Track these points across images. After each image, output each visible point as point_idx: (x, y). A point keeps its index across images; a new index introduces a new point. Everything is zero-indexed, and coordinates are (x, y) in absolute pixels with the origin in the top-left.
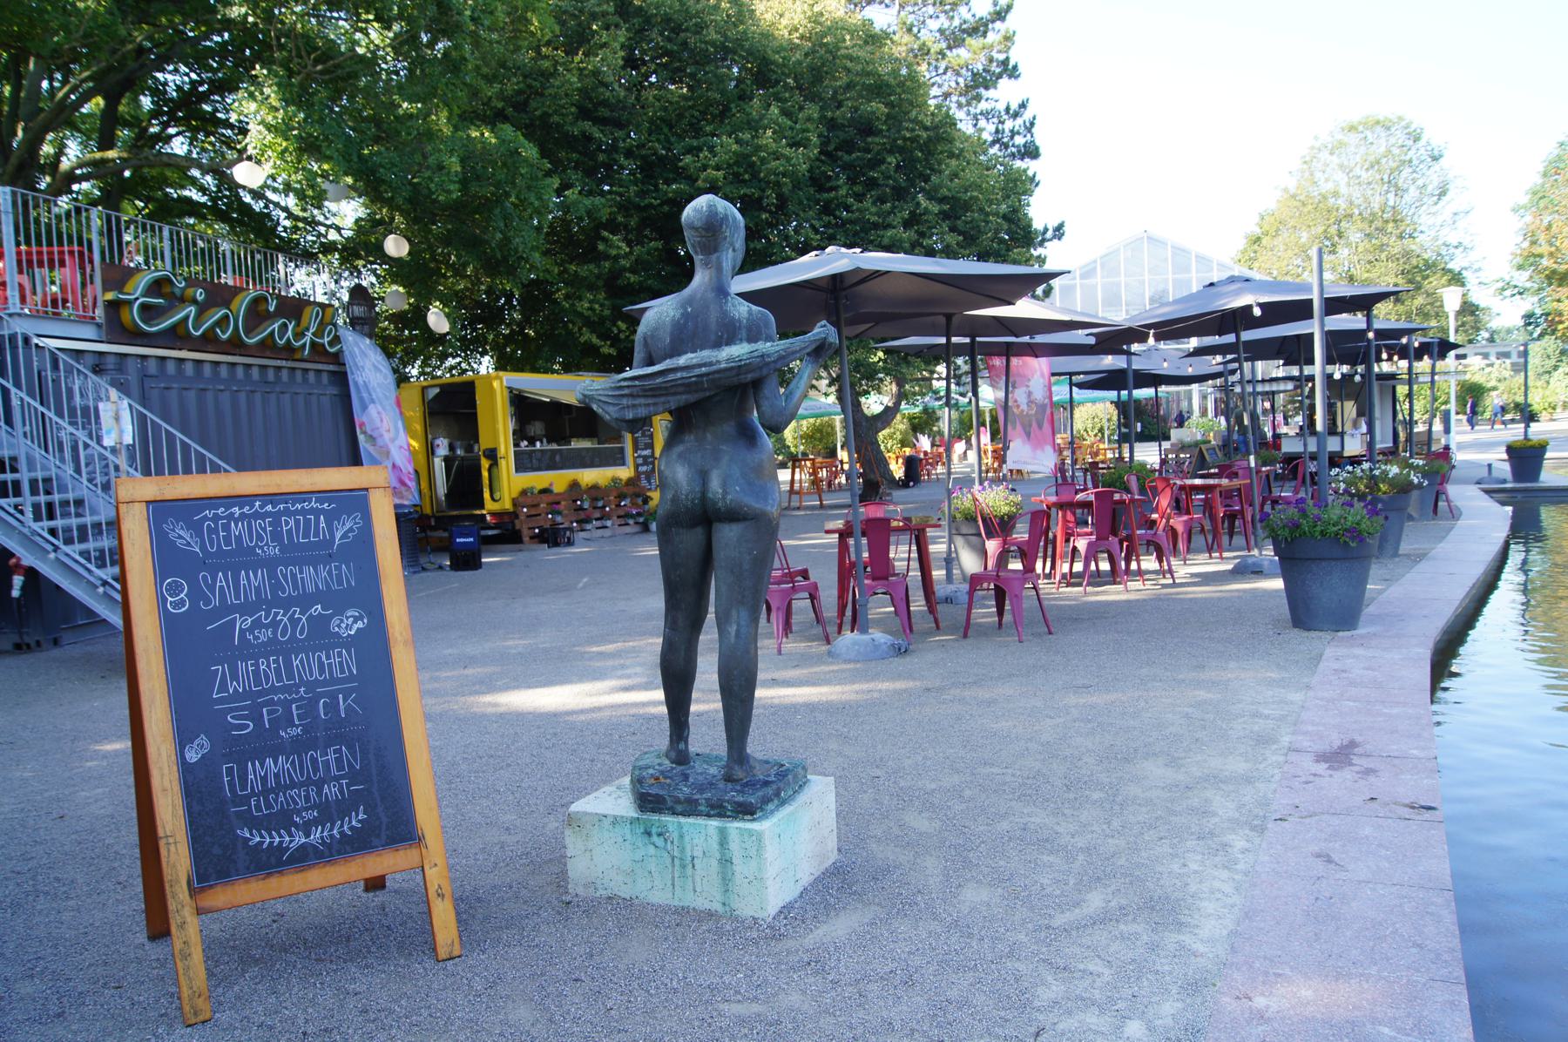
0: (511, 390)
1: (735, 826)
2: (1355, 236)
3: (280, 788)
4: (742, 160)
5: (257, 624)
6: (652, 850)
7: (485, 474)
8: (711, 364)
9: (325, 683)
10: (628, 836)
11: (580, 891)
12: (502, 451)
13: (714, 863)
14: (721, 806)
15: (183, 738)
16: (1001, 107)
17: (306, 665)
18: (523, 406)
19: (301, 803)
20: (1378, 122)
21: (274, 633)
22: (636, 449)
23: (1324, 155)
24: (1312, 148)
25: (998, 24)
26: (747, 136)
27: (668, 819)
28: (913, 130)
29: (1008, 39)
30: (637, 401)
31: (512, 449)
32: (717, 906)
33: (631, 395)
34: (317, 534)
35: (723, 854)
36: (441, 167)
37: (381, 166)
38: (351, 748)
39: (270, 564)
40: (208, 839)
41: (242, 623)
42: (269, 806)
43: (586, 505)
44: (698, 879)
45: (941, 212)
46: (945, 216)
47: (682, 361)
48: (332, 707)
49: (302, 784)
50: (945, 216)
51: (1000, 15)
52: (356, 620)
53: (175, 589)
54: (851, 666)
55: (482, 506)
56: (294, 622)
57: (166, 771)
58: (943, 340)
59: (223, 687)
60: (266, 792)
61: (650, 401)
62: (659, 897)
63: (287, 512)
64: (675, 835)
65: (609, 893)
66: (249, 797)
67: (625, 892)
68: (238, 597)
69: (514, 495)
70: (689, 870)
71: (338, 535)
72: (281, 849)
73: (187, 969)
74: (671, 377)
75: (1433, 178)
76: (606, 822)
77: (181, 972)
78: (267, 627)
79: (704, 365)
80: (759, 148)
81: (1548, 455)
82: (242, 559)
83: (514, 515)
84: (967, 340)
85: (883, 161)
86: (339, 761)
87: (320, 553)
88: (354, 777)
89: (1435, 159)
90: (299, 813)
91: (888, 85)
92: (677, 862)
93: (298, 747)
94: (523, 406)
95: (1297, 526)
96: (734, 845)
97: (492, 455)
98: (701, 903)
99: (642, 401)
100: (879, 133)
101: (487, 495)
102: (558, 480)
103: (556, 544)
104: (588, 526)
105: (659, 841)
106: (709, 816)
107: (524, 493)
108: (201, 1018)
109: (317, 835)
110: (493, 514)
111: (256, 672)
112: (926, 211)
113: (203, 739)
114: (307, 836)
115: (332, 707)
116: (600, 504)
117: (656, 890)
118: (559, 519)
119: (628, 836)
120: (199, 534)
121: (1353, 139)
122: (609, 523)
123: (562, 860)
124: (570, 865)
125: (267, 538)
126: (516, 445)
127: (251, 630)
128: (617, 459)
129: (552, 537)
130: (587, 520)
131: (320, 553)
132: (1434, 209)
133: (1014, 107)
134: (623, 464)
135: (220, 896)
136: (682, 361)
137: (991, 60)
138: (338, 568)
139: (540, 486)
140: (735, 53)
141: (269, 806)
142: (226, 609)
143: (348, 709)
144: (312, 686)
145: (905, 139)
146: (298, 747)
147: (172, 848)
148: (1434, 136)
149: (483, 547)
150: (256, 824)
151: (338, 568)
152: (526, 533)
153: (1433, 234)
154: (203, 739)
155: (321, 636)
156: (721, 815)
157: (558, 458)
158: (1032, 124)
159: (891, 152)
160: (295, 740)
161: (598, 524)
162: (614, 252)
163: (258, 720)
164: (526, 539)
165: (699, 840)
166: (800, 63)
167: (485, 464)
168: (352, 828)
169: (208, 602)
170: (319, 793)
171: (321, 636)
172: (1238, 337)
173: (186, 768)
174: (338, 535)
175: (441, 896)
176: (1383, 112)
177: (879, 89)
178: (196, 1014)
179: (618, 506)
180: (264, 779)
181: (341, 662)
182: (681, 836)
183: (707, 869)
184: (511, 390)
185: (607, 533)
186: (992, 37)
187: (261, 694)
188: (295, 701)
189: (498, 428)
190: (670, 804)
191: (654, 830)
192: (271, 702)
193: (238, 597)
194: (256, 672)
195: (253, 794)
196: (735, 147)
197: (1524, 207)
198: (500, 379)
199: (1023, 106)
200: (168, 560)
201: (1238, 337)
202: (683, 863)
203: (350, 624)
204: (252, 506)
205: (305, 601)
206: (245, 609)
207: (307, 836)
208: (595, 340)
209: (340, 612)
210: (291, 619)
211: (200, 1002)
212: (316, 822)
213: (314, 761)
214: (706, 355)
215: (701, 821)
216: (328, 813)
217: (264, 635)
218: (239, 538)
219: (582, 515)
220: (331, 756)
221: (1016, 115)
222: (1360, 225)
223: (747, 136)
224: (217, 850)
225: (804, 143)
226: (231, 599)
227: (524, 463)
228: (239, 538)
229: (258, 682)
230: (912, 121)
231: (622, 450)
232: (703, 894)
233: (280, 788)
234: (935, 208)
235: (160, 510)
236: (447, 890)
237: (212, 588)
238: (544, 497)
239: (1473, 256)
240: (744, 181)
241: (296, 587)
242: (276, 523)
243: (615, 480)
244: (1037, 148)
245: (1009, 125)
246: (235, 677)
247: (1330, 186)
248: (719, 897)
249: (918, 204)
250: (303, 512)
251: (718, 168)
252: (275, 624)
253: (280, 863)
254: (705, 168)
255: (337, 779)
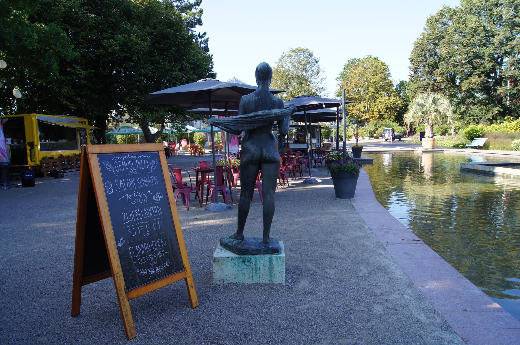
0: (38, 120)
1: (274, 256)
2: (294, 84)
3: (146, 254)
4: (125, 44)
5: (133, 198)
6: (245, 266)
7: (28, 152)
8: (270, 115)
9: (154, 218)
10: (237, 263)
11: (218, 283)
12: (36, 143)
13: (267, 268)
14: (268, 251)
15: (117, 240)
16: (197, 33)
17: (149, 212)
18: (42, 125)
19: (152, 259)
20: (301, 50)
21: (138, 201)
22: (81, 143)
23: (285, 58)
24: (282, 56)
25: (197, 7)
26: (126, 36)
27: (252, 257)
28: (181, 39)
29: (201, 12)
30: (244, 125)
31: (39, 143)
32: (268, 282)
33: (242, 123)
34: (146, 167)
35: (270, 265)
36: (30, 36)
37: (6, 33)
38: (163, 239)
39: (134, 176)
40: (128, 274)
41: (129, 197)
42: (143, 261)
43: (66, 163)
44: (261, 274)
45: (191, 67)
46: (192, 69)
47: (260, 112)
48: (156, 226)
49: (152, 253)
50: (192, 69)
51: (198, 4)
52: (160, 196)
53: (108, 185)
54: (216, 213)
55: (27, 164)
56: (143, 197)
57: (114, 251)
58: (208, 110)
59: (126, 221)
60: (142, 256)
61: (248, 125)
62: (247, 280)
63: (137, 159)
64: (254, 261)
65: (229, 282)
66: (137, 258)
67: (235, 281)
68: (127, 188)
69: (40, 159)
70: (258, 272)
71: (152, 167)
72: (148, 275)
73: (128, 320)
74: (257, 118)
75: (316, 68)
76: (229, 259)
77: (126, 321)
78: (136, 198)
79: (268, 115)
80: (131, 40)
81: (363, 150)
82: (125, 175)
83: (40, 167)
84: (224, 110)
85: (171, 49)
86: (160, 244)
87: (146, 173)
88: (165, 249)
89: (317, 62)
90: (152, 263)
91: (173, 23)
92: (254, 269)
93: (149, 240)
94: (42, 125)
95: (340, 168)
96: (274, 262)
97: (32, 145)
98: (262, 281)
99: (246, 125)
100: (170, 39)
101: (29, 159)
102: (55, 153)
103: (57, 177)
104: (67, 171)
105: (248, 264)
106: (264, 254)
107: (44, 158)
108: (134, 336)
109: (157, 269)
110: (31, 166)
111: (135, 214)
112: (186, 66)
113: (122, 239)
114: (155, 270)
115: (156, 226)
116: (71, 163)
117: (246, 279)
118: (57, 168)
119: (237, 263)
120: (113, 166)
121: (294, 54)
122: (74, 170)
123: (212, 273)
124: (214, 274)
125: (133, 167)
126: (40, 141)
127: (132, 199)
128: (75, 147)
129: (55, 175)
130: (67, 169)
131: (146, 173)
132: (316, 77)
133: (201, 34)
134: (77, 149)
135: (134, 294)
136: (260, 112)
137: (195, 18)
138: (153, 178)
139: (49, 156)
140: (120, 6)
141: (143, 261)
142: (124, 193)
143: (161, 226)
144: (151, 218)
145: (178, 42)
146: (149, 240)
147: (119, 278)
148: (316, 55)
149: (35, 179)
150: (140, 267)
151: (153, 178)
152: (45, 173)
153: (315, 84)
154: (122, 239)
155: (151, 202)
156: (268, 254)
157: (55, 146)
158: (207, 40)
159: (173, 46)
160: (148, 237)
161: (70, 170)
162: (78, 72)
163: (137, 231)
164: (45, 176)
165: (262, 262)
166: (142, 12)
167: (28, 148)
168: (166, 266)
169: (118, 190)
170: (156, 255)
171: (151, 202)
172: (305, 112)
173: (119, 249)
174: (152, 167)
175: (192, 287)
176: (302, 47)
177: (170, 24)
178: (132, 335)
179: (76, 164)
180: (141, 251)
181: (157, 210)
182: (256, 261)
183: (264, 271)
184: (38, 120)
185: (73, 173)
186: (194, 11)
187: (137, 222)
188: (146, 224)
189: (34, 135)
190: (250, 251)
191: (246, 260)
192: (140, 225)
193: (127, 188)
194: (135, 214)
195: (139, 257)
196: (122, 39)
197: (339, 78)
198: (35, 116)
199: (204, 34)
200: (106, 175)
201: (305, 112)
202: (256, 270)
203: (158, 198)
204: (127, 156)
205: (146, 189)
206: (130, 192)
207: (155, 270)
208: (68, 103)
209: (155, 193)
210: (142, 195)
211: (132, 331)
212: (157, 265)
213: (154, 244)
214: (266, 111)
215: (262, 256)
216: (160, 262)
217: (135, 201)
218: (125, 167)
219: (65, 167)
220: (158, 243)
221: (201, 37)
222: (296, 80)
223: (126, 36)
224: (131, 278)
225: (147, 40)
226: (125, 189)
227: (44, 148)
228: (125, 167)
229: (136, 219)
230: (181, 36)
231: (77, 144)
232: (263, 278)
233: (146, 254)
234: (189, 66)
235: (102, 156)
236: (193, 286)
237: (119, 185)
238: (52, 160)
239: (326, 92)
240: (125, 51)
241: (142, 185)
242: (134, 162)
243: (75, 154)
244: (208, 49)
245: (199, 40)
246: (129, 217)
247: (287, 68)
248: (268, 279)
249: (183, 64)
250: (142, 159)
251: (116, 46)
252: (138, 197)
253: (149, 280)
254: (111, 45)
255: (161, 250)
